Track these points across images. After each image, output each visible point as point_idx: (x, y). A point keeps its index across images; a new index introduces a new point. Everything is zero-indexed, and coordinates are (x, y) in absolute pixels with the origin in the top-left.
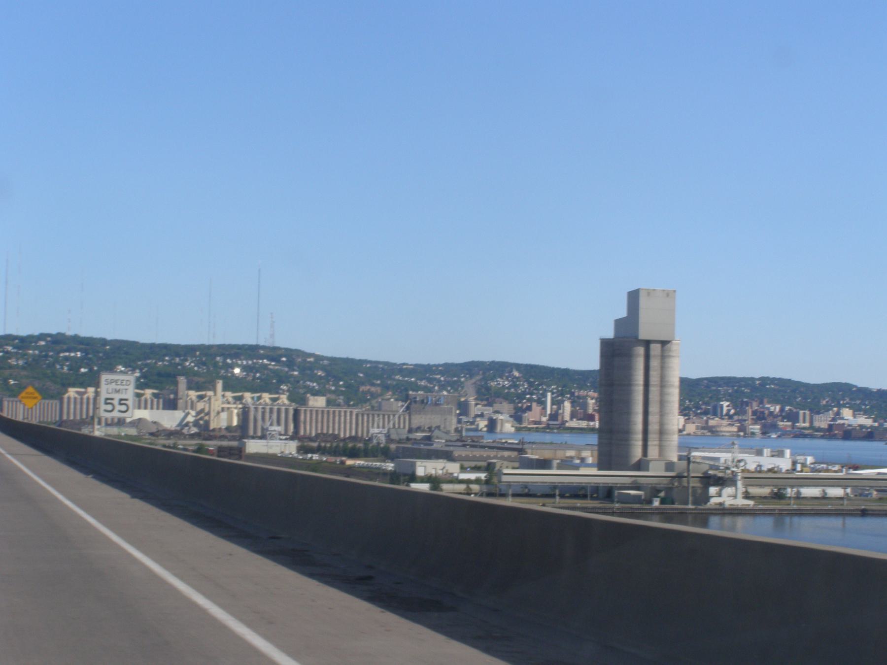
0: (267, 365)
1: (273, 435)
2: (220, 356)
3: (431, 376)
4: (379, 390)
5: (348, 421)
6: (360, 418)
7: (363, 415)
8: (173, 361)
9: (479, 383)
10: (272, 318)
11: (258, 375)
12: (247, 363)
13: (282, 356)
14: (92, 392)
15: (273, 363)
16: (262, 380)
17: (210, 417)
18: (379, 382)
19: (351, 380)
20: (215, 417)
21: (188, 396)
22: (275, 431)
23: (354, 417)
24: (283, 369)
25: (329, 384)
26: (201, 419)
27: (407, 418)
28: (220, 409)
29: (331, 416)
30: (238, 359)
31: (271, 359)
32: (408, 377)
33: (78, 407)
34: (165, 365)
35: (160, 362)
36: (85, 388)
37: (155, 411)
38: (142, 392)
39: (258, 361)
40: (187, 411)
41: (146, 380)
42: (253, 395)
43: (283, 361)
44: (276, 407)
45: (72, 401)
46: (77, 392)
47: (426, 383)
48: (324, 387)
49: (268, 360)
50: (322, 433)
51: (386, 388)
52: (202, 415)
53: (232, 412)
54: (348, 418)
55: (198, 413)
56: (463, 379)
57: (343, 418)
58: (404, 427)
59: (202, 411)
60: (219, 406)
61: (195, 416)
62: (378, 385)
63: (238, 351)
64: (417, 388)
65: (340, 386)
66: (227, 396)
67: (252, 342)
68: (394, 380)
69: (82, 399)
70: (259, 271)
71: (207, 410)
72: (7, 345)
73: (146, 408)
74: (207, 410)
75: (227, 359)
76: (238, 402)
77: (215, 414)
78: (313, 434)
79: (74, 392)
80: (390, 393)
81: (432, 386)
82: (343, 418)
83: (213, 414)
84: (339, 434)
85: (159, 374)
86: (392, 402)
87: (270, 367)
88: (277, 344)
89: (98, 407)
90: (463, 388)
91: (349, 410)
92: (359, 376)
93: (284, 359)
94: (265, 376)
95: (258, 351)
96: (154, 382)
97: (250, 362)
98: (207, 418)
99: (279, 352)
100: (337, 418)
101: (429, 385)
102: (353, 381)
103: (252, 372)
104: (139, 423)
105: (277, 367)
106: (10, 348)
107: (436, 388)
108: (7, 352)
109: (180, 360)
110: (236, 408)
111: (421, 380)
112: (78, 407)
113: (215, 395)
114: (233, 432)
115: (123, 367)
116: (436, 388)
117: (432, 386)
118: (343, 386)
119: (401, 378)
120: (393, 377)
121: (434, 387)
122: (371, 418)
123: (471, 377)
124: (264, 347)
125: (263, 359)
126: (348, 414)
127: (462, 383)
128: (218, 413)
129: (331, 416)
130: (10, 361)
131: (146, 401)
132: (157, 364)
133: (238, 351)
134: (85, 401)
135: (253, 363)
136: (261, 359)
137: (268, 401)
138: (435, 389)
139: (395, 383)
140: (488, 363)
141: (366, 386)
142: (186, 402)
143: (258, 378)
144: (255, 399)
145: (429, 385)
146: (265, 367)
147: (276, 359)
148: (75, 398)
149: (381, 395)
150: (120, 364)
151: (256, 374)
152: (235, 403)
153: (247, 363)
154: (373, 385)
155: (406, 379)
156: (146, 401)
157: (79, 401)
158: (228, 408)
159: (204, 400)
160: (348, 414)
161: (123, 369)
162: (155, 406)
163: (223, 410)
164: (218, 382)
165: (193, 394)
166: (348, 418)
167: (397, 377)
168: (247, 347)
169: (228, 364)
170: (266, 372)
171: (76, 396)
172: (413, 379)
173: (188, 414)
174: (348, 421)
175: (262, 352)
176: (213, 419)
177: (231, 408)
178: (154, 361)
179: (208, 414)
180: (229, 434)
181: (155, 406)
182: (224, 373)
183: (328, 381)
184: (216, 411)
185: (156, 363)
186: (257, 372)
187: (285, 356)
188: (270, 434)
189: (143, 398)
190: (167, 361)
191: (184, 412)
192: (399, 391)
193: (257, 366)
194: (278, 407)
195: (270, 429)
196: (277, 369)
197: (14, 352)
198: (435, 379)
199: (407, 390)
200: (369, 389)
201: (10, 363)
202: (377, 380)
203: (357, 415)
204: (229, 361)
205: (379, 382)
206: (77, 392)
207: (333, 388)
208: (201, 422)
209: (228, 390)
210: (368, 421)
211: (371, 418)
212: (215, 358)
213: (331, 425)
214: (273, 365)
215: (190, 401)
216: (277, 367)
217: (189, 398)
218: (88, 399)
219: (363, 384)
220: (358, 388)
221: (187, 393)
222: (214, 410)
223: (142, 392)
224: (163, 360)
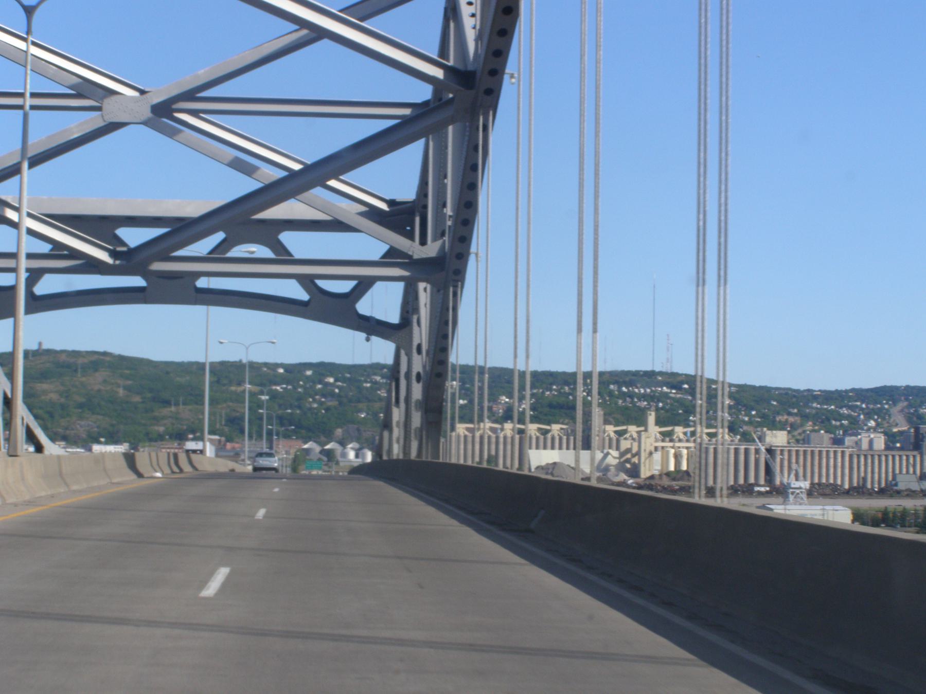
0: (667, 393)
1: (798, 494)
2: (613, 384)
3: (850, 404)
4: (798, 419)
5: (839, 464)
6: (855, 460)
7: (858, 456)
8: (562, 391)
9: (906, 410)
10: (668, 340)
11: (661, 405)
12: (645, 391)
13: (683, 383)
14: (510, 429)
15: (674, 391)
16: (667, 411)
17: (639, 459)
18: (796, 411)
19: (765, 409)
20: (646, 459)
21: (604, 432)
22: (800, 488)
23: (847, 459)
24: (685, 397)
25: (741, 414)
26: (628, 461)
27: (918, 459)
28: (653, 449)
29: (817, 458)
30: (634, 387)
31: (672, 387)
32: (827, 405)
33: (470, 447)
34: (554, 395)
35: (547, 391)
36: (549, 423)
37: (564, 451)
38: (548, 427)
39: (657, 388)
40: (605, 451)
41: (536, 413)
42: (686, 430)
43: (685, 389)
44: (733, 447)
45: (462, 439)
46: (468, 429)
47: (850, 411)
48: (738, 417)
49: (667, 388)
50: (819, 484)
51: (805, 417)
52: (629, 456)
53: (668, 452)
54: (839, 460)
55: (622, 454)
56: (886, 406)
57: (832, 461)
58: (914, 472)
59: (628, 451)
60: (651, 445)
61: (620, 458)
62: (796, 414)
63: (634, 378)
64: (841, 417)
65: (754, 416)
66: (630, 431)
67: (648, 368)
68: (813, 408)
69: (497, 438)
70: (654, 287)
71: (635, 450)
72: (375, 374)
73: (553, 448)
74: (635, 450)
75: (622, 387)
76: (667, 439)
77: (647, 456)
78: (847, 486)
79: (463, 428)
80: (810, 423)
81: (856, 414)
82: (832, 461)
83: (643, 455)
84: (842, 485)
85: (551, 406)
86: (823, 434)
87: (672, 395)
88: (675, 370)
89: (880, 515)
90: (890, 416)
91: (839, 450)
92: (773, 405)
93: (686, 386)
94: (669, 406)
95: (656, 378)
96: (546, 415)
97: (648, 390)
98: (635, 460)
99: (680, 379)
100: (824, 461)
101: (853, 413)
102: (766, 410)
103: (653, 401)
104: (553, 468)
105: (679, 396)
106: (378, 378)
107: (862, 417)
108: (376, 383)
109: (570, 389)
110: (673, 447)
111: (841, 408)
112: (470, 447)
113: (646, 430)
114: (678, 480)
115: (507, 398)
116: (862, 417)
117: (856, 414)
118: (757, 415)
119: (819, 406)
120: (810, 404)
121: (859, 415)
122: (869, 461)
123: (895, 403)
124: (661, 373)
125: (662, 387)
126: (839, 455)
127: (887, 410)
128: (651, 454)
129: (817, 458)
130: (379, 392)
131: (553, 439)
132: (545, 394)
133: (634, 378)
134: (501, 440)
135: (652, 391)
136: (659, 387)
137: (612, 435)
138: (860, 418)
139: (814, 411)
140: (903, 388)
141: (783, 415)
142: (604, 439)
143: (662, 408)
144: (689, 434)
145: (853, 413)
146: (666, 395)
147: (678, 387)
148: (465, 437)
149: (802, 425)
150: (504, 394)
151: (658, 404)
152: (663, 441)
153: (645, 391)
154: (790, 414)
155: (825, 407)
156: (553, 439)
157: (470, 439)
158: (663, 448)
159: (625, 436)
160: (839, 455)
161: (507, 400)
162: (564, 445)
163: (656, 449)
164: (650, 414)
165: (610, 429)
166: (839, 460)
167: (815, 405)
168: (642, 373)
169: (624, 393)
170: (669, 401)
171: (467, 433)
172: (833, 407)
173: (608, 454)
174: (839, 464)
175: (660, 378)
176: (644, 463)
177: (667, 447)
178: (541, 391)
179: (638, 454)
180: (674, 483)
181: (564, 445)
182: (622, 403)
183: (740, 411)
184: (648, 451)
185: (543, 393)
186: (659, 401)
187: (687, 383)
188: (793, 493)
189: (549, 436)
190: (555, 390)
191: (602, 452)
192: (820, 420)
193: (657, 394)
194: (714, 446)
195: (793, 486)
196: (680, 398)
197: (383, 383)
198: (857, 406)
199: (828, 420)
200: (787, 420)
201: (379, 395)
202: (794, 408)
203: (851, 456)
204: (624, 389)
205: (796, 411)
206: (468, 429)
207: (746, 419)
208: (628, 466)
209: (610, 423)
210: (866, 465)
211: (869, 461)
212: (608, 386)
213: (816, 470)
214: (674, 393)
215: (607, 438)
216: (679, 396)
217: (606, 434)
218: (505, 438)
219: (778, 414)
220: (774, 417)
221: (604, 429)
222: (645, 450)
223: (548, 427)
224: (551, 390)
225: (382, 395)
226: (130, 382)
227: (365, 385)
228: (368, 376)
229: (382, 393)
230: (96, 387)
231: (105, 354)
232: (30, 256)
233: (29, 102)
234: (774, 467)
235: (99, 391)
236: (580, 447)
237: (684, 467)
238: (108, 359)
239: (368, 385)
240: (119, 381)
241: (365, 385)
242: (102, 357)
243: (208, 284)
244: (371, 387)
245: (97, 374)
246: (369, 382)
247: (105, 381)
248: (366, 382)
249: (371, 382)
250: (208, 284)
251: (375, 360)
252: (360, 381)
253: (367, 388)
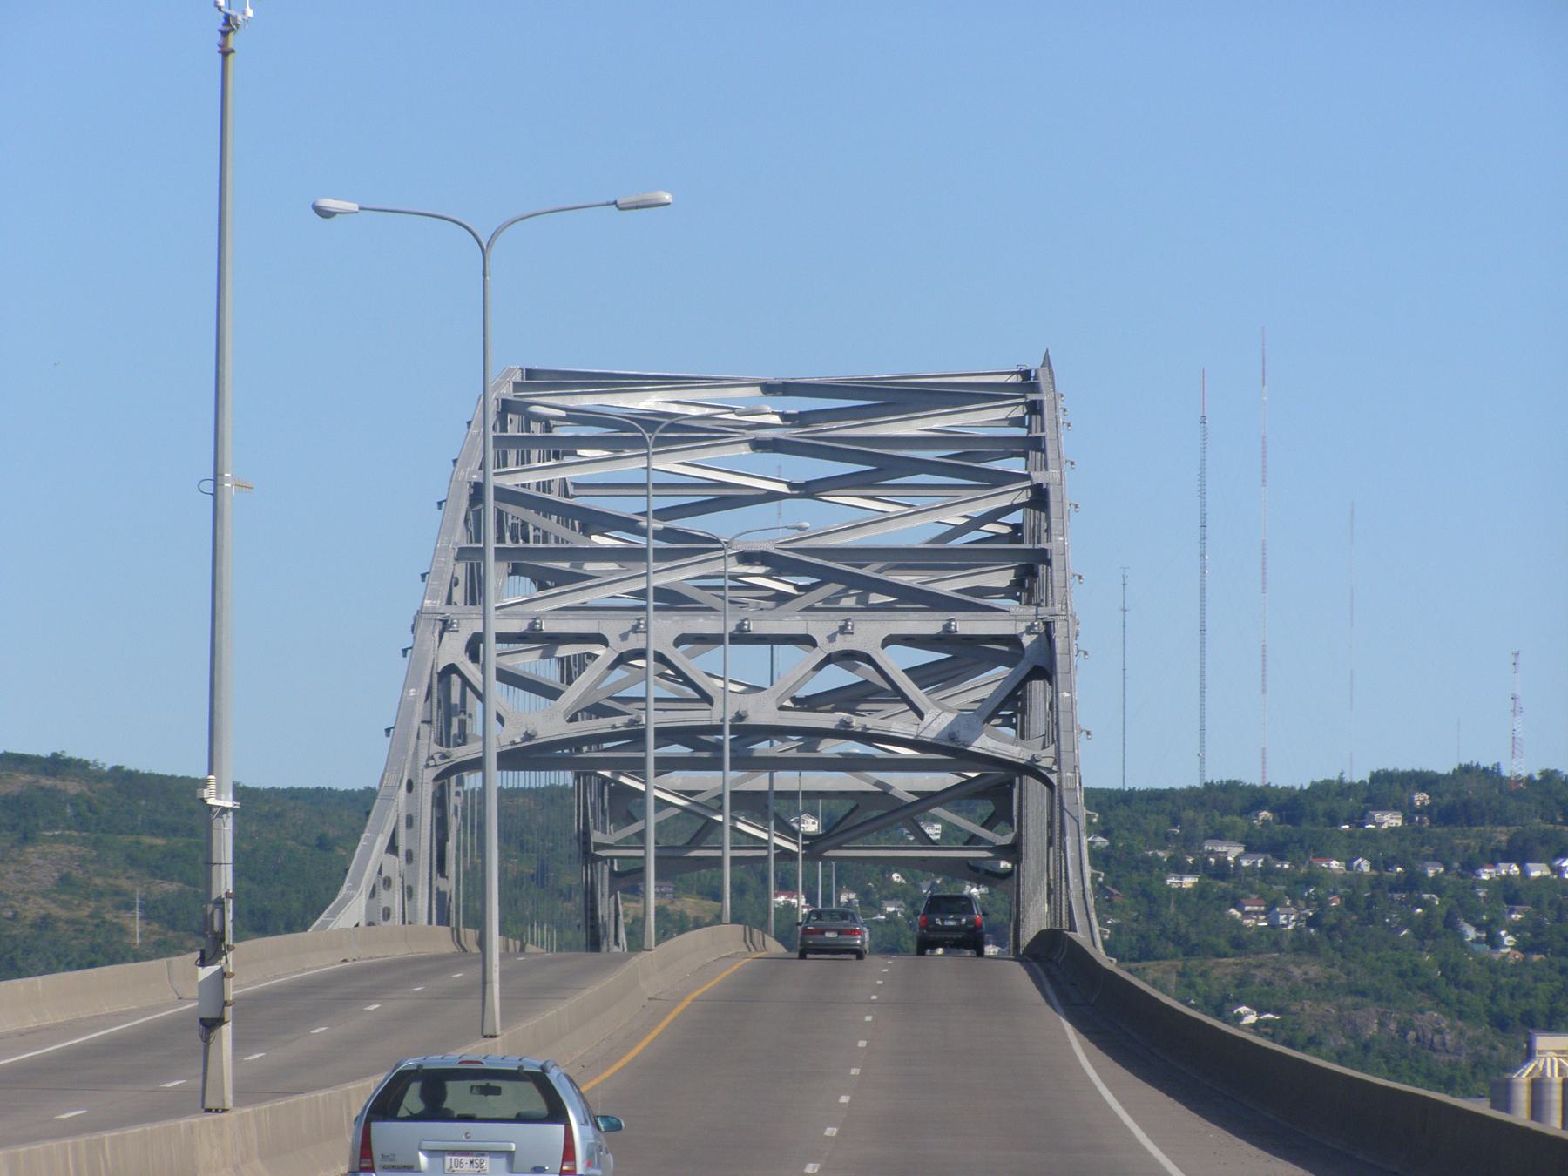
72: (1219, 836)
106: (1232, 852)
108: (1222, 870)
201: (1237, 924)
225: (1249, 922)
226: (172, 887)
227: (1172, 881)
228: (1189, 842)
229: (1247, 914)
230: (33, 909)
231: (57, 765)
232: (657, 700)
233: (652, 491)
234: (1078, 1038)
235: (45, 923)
236: (733, 855)
237: (671, 889)
238: (72, 787)
239: (1189, 881)
240: (125, 884)
241: (1172, 881)
242: (47, 782)
243: (772, 649)
244: (1200, 891)
245: (32, 853)
246: (1192, 871)
247: (65, 881)
248: (1180, 869)
249: (1197, 868)
250: (772, 649)
251: (1218, 773)
252: (1150, 864)
253: (1181, 895)
